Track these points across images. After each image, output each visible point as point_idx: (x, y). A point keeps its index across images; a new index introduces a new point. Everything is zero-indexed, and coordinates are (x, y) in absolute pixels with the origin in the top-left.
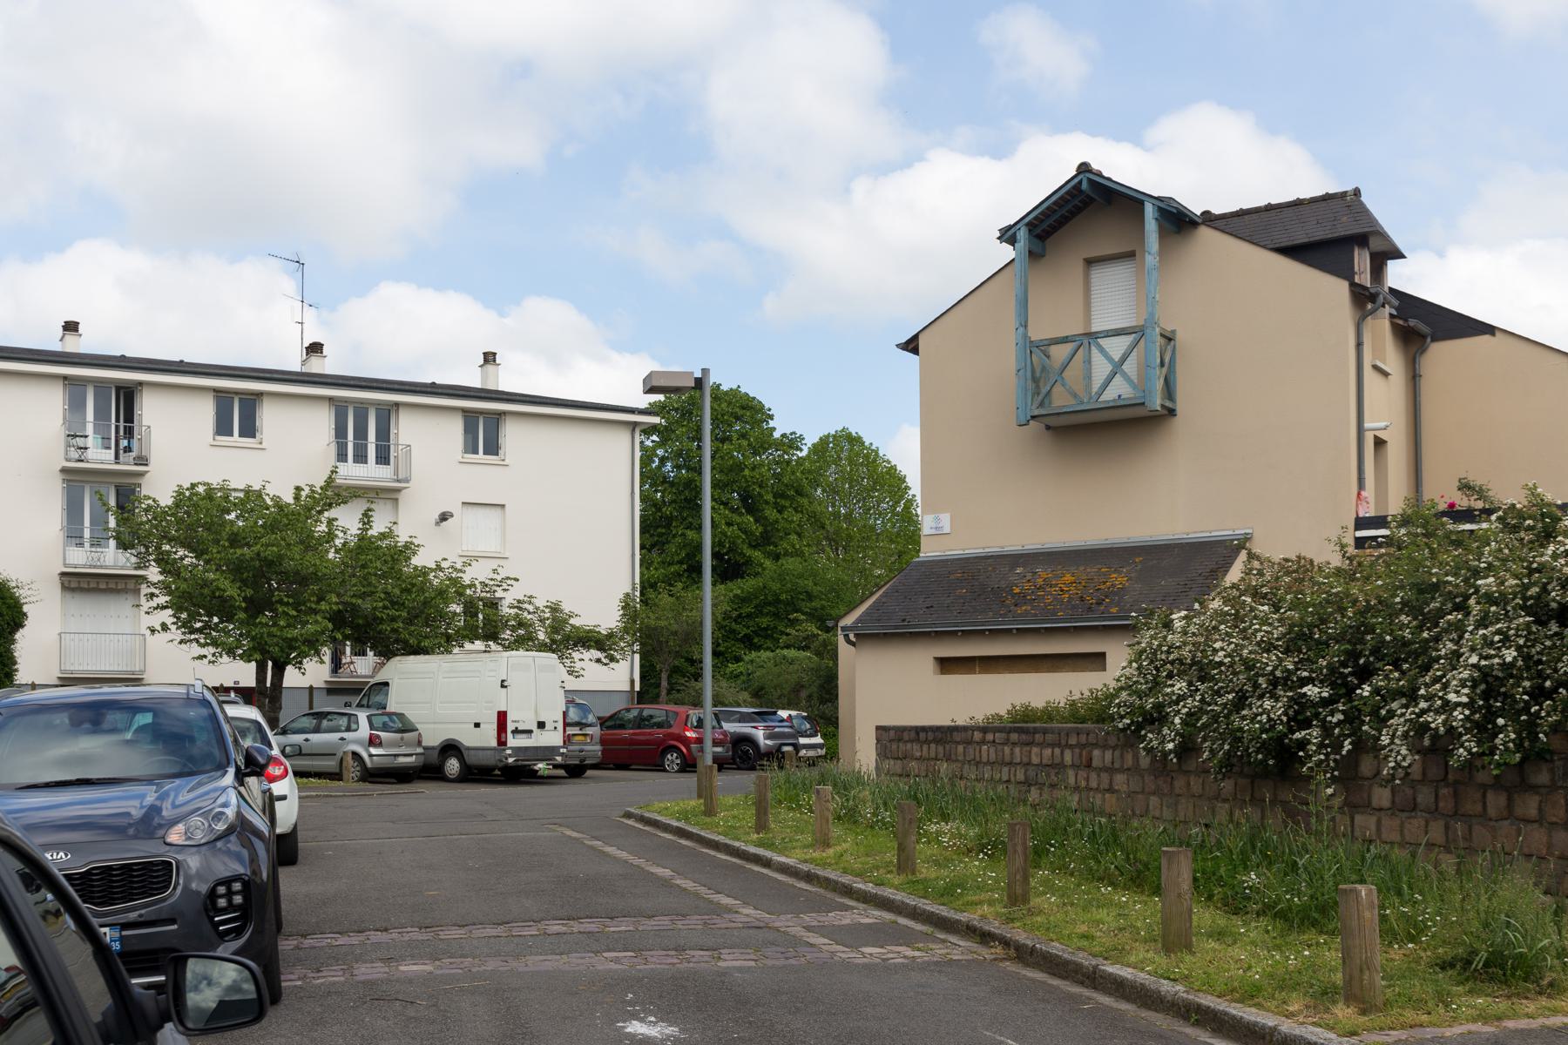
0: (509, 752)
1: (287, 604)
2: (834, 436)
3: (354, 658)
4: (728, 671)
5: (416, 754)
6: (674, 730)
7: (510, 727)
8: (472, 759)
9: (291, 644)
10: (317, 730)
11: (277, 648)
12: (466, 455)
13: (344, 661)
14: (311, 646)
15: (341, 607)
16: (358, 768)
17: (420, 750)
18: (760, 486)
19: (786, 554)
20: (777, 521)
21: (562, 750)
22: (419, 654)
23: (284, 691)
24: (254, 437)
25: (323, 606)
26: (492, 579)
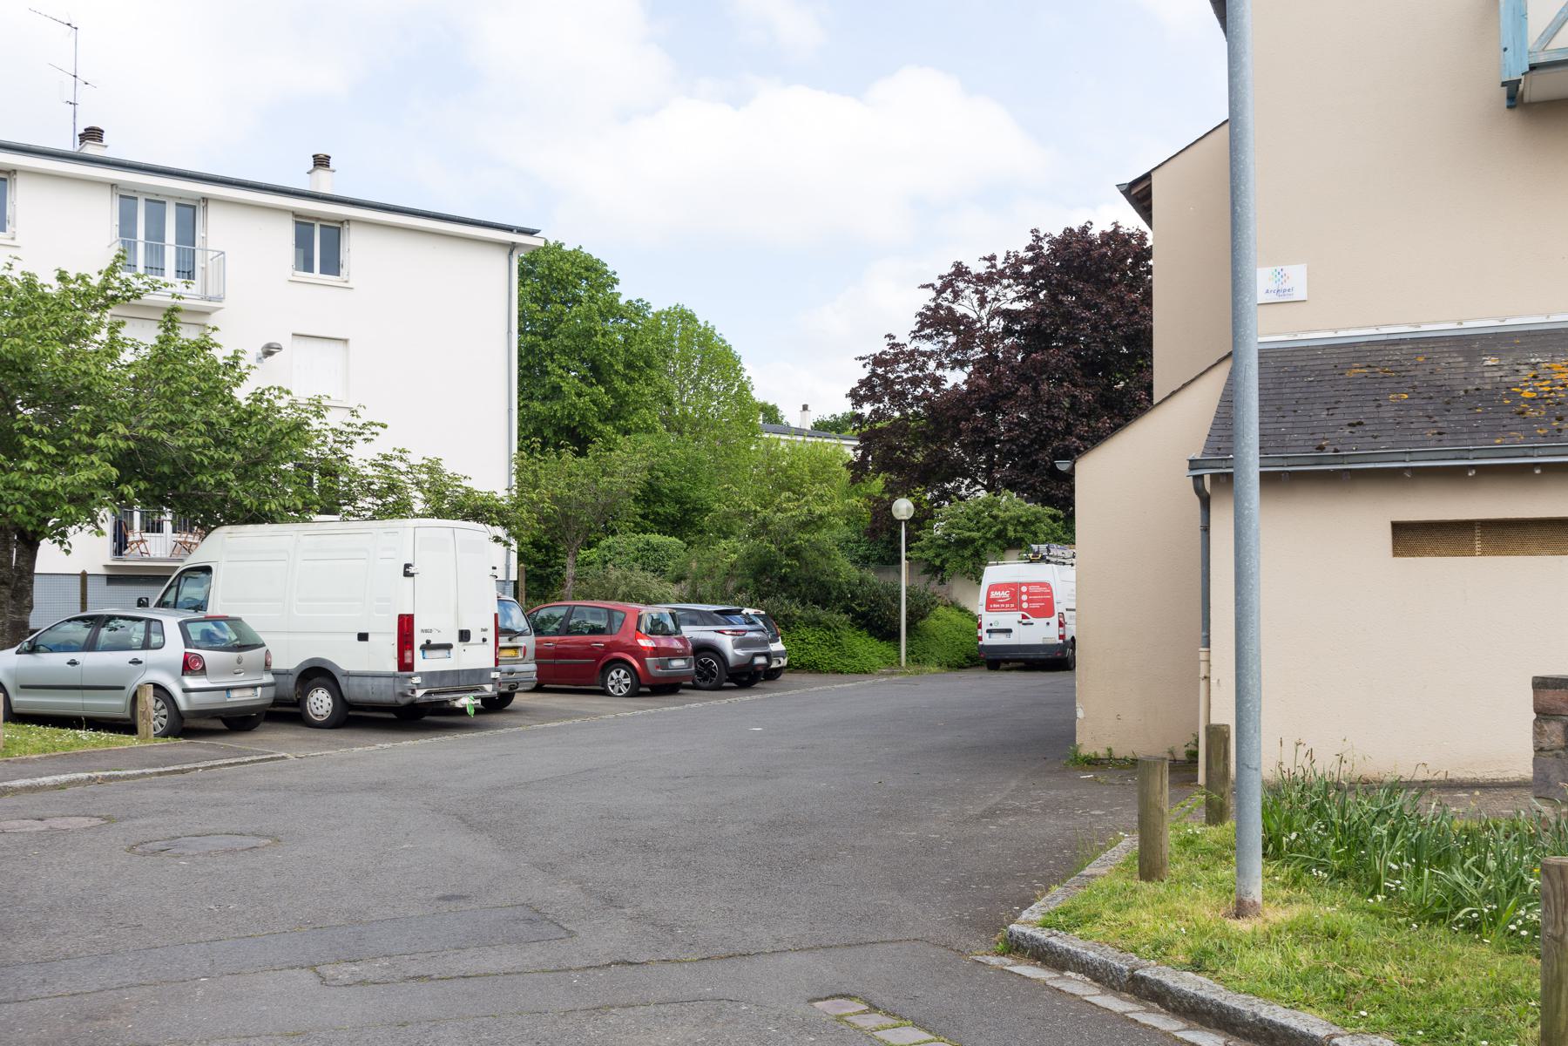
0: (417, 680)
1: (41, 436)
2: (668, 313)
3: (146, 536)
4: (580, 558)
5: (262, 686)
6: (626, 640)
7: (419, 640)
8: (353, 691)
9: (45, 502)
10: (91, 646)
11: (20, 509)
12: (298, 273)
13: (131, 539)
14: (82, 503)
15: (132, 444)
16: (164, 712)
17: (268, 678)
18: (611, 355)
19: (638, 430)
20: (627, 394)
21: (493, 675)
22: (263, 522)
23: (36, 579)
24: (5, 231)
25: (102, 440)
26: (349, 425)
